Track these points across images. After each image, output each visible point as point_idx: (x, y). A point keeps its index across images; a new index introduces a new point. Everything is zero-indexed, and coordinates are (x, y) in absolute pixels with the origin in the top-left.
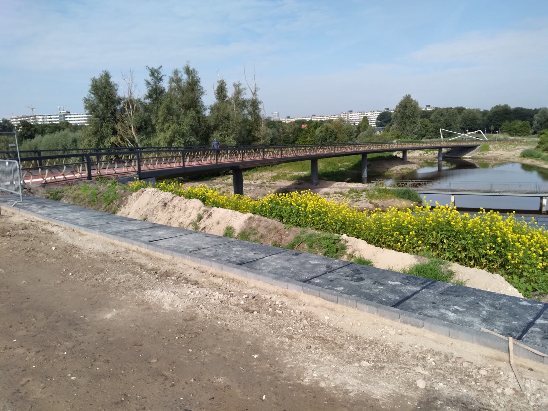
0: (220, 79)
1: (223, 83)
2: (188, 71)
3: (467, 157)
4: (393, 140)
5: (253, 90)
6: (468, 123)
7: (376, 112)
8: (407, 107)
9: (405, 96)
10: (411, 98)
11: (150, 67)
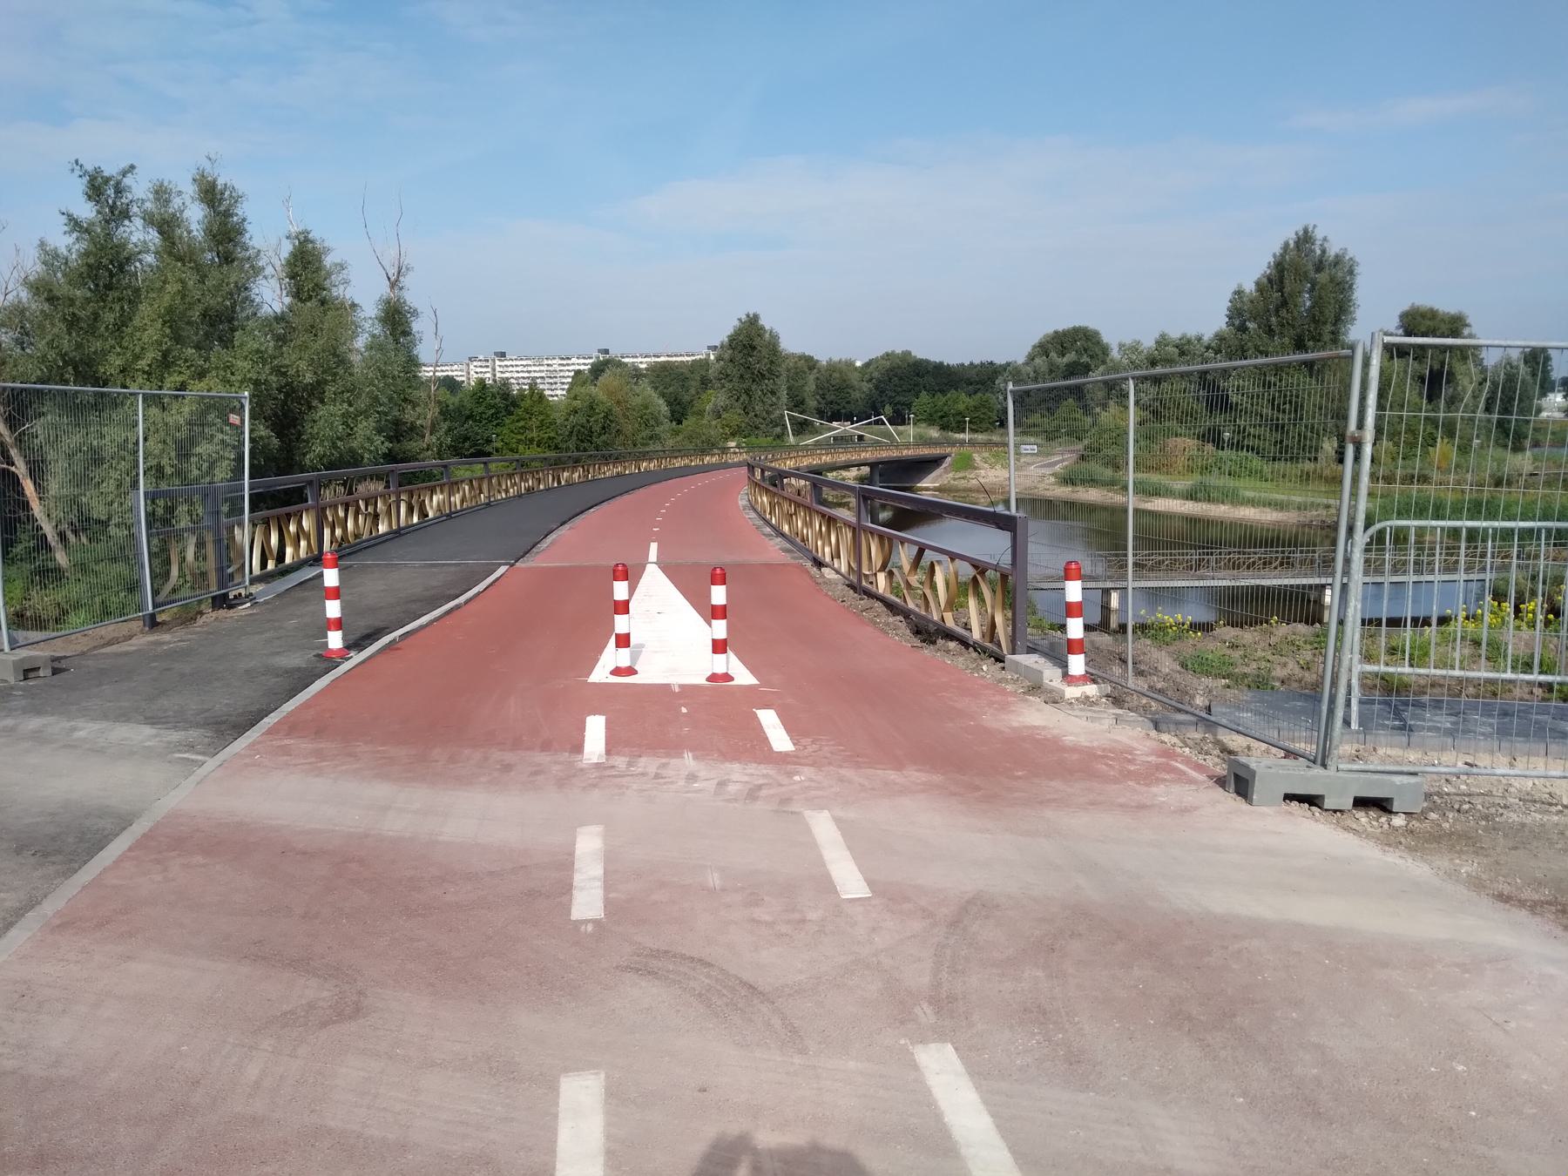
0: (294, 229)
1: (307, 240)
2: (210, 193)
3: (928, 486)
4: (726, 439)
5: (392, 271)
6: (830, 397)
7: (574, 360)
8: (750, 348)
9: (744, 318)
10: (762, 322)
11: (89, 168)
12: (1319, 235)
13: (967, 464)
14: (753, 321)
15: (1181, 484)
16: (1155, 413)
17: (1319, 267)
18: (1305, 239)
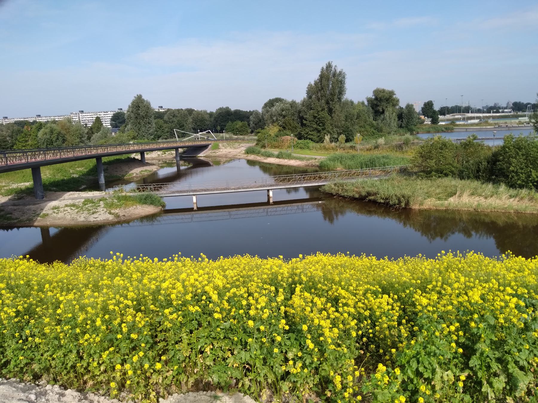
3: (202, 155)
4: (129, 141)
6: (198, 124)
7: (109, 113)
8: (139, 106)
9: (136, 96)
12: (333, 65)
13: (217, 147)
14: (139, 98)
15: (276, 152)
16: (284, 128)
17: (334, 75)
18: (329, 66)
